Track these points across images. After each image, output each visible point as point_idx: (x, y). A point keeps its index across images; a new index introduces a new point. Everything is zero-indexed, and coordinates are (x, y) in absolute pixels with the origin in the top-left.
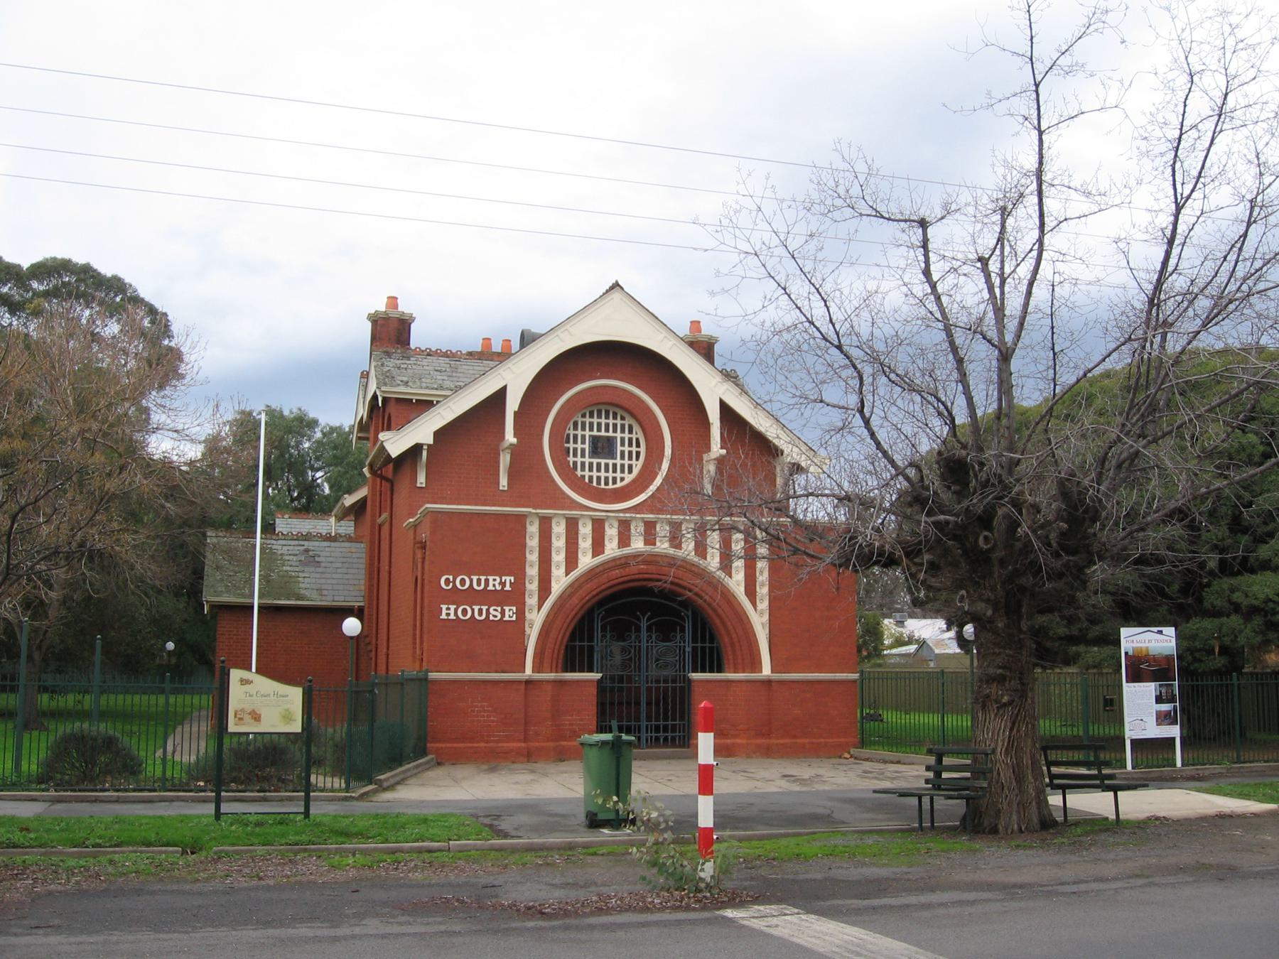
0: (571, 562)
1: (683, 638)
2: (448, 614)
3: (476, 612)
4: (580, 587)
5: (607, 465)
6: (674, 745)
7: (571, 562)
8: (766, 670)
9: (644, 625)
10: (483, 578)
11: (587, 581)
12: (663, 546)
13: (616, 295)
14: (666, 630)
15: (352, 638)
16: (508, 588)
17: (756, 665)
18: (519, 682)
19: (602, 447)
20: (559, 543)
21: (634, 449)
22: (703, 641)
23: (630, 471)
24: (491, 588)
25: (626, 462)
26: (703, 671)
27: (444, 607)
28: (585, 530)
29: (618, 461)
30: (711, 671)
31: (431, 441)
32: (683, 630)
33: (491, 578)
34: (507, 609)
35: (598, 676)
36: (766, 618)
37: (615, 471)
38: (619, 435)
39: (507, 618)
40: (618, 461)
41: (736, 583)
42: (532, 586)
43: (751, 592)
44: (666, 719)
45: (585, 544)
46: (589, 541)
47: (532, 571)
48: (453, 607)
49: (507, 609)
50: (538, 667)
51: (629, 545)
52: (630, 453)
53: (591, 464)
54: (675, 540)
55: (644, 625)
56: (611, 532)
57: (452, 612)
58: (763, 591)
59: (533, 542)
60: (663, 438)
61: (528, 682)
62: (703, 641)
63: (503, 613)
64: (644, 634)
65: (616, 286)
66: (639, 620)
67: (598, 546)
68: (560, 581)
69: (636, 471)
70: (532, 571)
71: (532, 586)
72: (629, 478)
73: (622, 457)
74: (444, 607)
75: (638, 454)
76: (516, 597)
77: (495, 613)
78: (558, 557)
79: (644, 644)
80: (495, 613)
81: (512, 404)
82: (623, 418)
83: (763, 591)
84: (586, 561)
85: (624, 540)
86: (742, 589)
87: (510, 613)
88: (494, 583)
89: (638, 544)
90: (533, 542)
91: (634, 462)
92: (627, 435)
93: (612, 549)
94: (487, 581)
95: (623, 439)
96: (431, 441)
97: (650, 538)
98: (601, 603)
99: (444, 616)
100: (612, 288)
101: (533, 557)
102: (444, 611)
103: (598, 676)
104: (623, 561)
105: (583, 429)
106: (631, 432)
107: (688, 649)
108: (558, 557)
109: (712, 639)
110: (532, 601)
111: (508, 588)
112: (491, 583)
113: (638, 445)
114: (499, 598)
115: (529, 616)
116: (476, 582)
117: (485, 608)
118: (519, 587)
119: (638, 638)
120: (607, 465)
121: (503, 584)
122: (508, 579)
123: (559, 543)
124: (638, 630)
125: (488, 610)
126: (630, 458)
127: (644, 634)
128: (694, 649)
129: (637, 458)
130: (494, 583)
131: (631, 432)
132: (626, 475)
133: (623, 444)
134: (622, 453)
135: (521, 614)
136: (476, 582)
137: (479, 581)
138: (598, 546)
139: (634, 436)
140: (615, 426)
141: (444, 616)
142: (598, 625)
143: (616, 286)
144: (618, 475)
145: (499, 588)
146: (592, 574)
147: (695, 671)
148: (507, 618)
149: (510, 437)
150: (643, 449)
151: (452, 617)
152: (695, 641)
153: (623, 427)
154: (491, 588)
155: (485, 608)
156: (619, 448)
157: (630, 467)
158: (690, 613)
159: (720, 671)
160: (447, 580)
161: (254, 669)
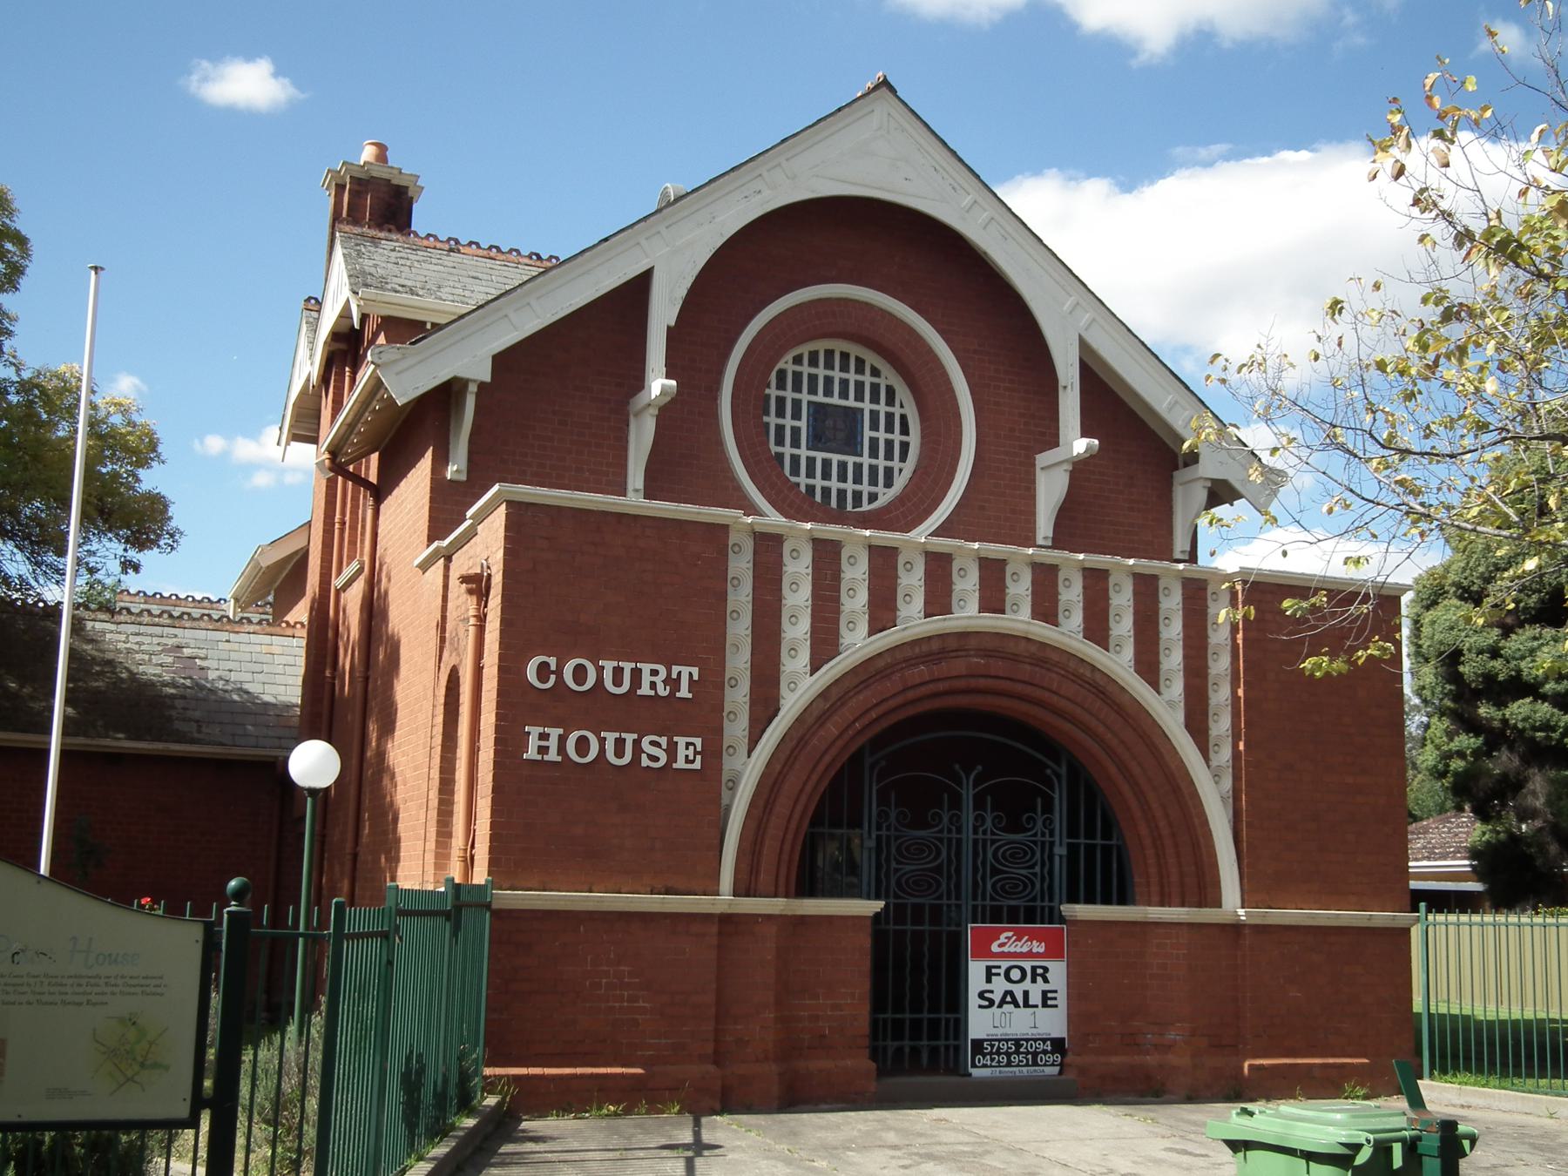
0: (824, 644)
1: (1048, 823)
2: (543, 750)
3: (607, 745)
4: (842, 700)
5: (843, 466)
6: (916, 1069)
7: (824, 644)
8: (1232, 905)
9: (968, 793)
10: (628, 667)
11: (865, 684)
12: (1019, 619)
13: (884, 105)
14: (1015, 808)
15: (313, 792)
16: (684, 692)
17: (1208, 894)
18: (707, 917)
19: (835, 429)
20: (798, 597)
21: (897, 437)
22: (1090, 834)
23: (889, 483)
24: (645, 690)
25: (881, 463)
26: (1090, 900)
27: (534, 731)
28: (856, 574)
29: (866, 460)
30: (1107, 901)
31: (486, 376)
32: (1048, 808)
33: (646, 668)
34: (681, 741)
35: (878, 905)
36: (1227, 783)
37: (858, 479)
38: (867, 406)
39: (680, 764)
40: (866, 460)
41: (1166, 707)
42: (738, 697)
43: (1197, 723)
44: (916, 1008)
45: (855, 601)
46: (863, 596)
47: (739, 662)
48: (555, 733)
49: (681, 741)
50: (743, 888)
51: (947, 610)
52: (889, 444)
53: (811, 462)
54: (1046, 609)
55: (968, 793)
56: (912, 582)
57: (553, 743)
58: (1221, 725)
59: (741, 598)
60: (958, 416)
61: (727, 921)
62: (1090, 834)
63: (672, 751)
64: (968, 816)
65: (885, 83)
66: (960, 784)
67: (882, 611)
68: (801, 686)
69: (900, 482)
70: (739, 662)
71: (738, 697)
72: (886, 496)
73: (874, 453)
74: (534, 731)
75: (905, 447)
76: (700, 717)
77: (653, 751)
78: (797, 630)
79: (968, 836)
80: (653, 751)
81: (663, 311)
82: (875, 372)
83: (1221, 725)
84: (858, 642)
85: (938, 601)
86: (1180, 716)
87: (688, 753)
88: (653, 679)
89: (967, 613)
90: (741, 598)
91: (896, 464)
92: (882, 408)
93: (913, 620)
94: (636, 674)
95: (874, 415)
96: (486, 376)
97: (993, 599)
98: (877, 742)
99: (531, 753)
100: (876, 88)
101: (740, 630)
102: (533, 743)
103: (878, 905)
104: (935, 646)
105: (797, 387)
106: (890, 401)
107: (1060, 850)
108: (797, 630)
109: (1109, 828)
110: (736, 728)
111: (684, 692)
112: (646, 678)
113: (905, 430)
114: (663, 715)
115: (730, 764)
116: (607, 673)
117: (630, 738)
118: (711, 686)
119: (956, 821)
120: (843, 466)
121: (674, 683)
122: (687, 673)
123: (798, 597)
124: (956, 802)
125: (637, 743)
126: (889, 456)
127: (968, 816)
128: (1073, 850)
129: (903, 458)
130: (653, 679)
131: (890, 401)
132: (880, 489)
133: (874, 426)
134: (874, 442)
135: (713, 753)
136: (607, 673)
137: (618, 672)
138: (882, 611)
139: (897, 411)
140: (860, 386)
141: (531, 753)
142: (871, 792)
143: (885, 83)
144: (865, 488)
145: (663, 691)
146: (869, 672)
147: (1073, 899)
148: (680, 764)
149: (658, 384)
150: (914, 439)
151: (553, 756)
152: (1073, 832)
153: (875, 389)
154: (645, 690)
155: (630, 738)
156: (868, 434)
157: (889, 472)
158: (1063, 771)
159: (1123, 901)
160: (543, 667)
161: (44, 868)
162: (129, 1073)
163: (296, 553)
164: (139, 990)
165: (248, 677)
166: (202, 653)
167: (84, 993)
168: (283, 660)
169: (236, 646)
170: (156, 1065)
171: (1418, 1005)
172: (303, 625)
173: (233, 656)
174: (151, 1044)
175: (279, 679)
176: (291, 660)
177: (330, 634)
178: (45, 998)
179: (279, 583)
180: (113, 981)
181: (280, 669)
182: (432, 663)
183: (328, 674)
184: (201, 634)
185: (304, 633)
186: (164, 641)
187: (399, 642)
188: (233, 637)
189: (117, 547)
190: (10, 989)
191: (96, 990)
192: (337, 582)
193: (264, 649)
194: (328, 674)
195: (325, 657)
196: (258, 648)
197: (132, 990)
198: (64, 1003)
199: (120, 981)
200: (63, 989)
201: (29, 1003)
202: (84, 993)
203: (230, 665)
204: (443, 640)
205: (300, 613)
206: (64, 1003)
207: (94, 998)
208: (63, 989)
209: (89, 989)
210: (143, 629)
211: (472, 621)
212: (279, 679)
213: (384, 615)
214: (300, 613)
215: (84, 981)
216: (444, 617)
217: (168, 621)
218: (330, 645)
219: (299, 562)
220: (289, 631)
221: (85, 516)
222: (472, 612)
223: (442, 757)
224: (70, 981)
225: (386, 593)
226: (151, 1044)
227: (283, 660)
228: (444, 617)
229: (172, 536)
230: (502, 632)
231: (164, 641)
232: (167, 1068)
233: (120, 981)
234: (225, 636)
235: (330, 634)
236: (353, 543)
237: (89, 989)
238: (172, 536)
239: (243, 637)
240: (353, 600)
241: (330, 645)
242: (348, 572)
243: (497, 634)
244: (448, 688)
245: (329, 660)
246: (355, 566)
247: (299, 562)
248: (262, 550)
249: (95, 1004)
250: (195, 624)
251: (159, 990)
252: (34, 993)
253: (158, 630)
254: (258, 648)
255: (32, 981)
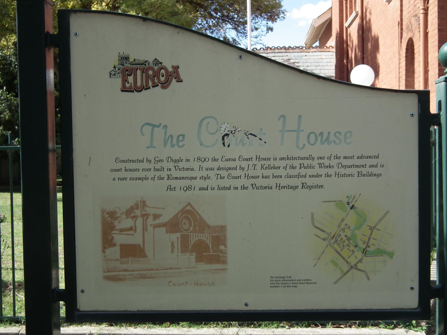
162: (353, 261)
163: (326, 21)
164: (354, 171)
165: (314, 68)
166: (297, 61)
167: (299, 176)
168: (326, 60)
169: (309, 57)
170: (380, 252)
171: (18, 198)
172: (332, 47)
173: (308, 61)
174: (372, 229)
175: (325, 68)
176: (329, 60)
177: (345, 45)
178: (260, 182)
179: (322, 32)
180: (326, 162)
181: (326, 64)
182: (397, 41)
183: (345, 62)
184: (296, 54)
185: (334, 50)
186: (283, 58)
187: (378, 38)
188: (307, 54)
189: (264, 22)
190: (224, 173)
191: (310, 172)
192: (346, 25)
193: (319, 57)
194: (345, 62)
195: (343, 55)
196: (317, 57)
197: (348, 171)
198: (279, 187)
199: (334, 162)
200: (277, 172)
201: (244, 188)
202: (299, 176)
203: (307, 64)
204: (402, 29)
205: (332, 42)
206: (279, 187)
207: (310, 181)
208: (277, 172)
209: (303, 172)
210: (276, 54)
211: (422, 11)
212: (325, 68)
213: (369, 29)
214: (332, 42)
215: (296, 163)
216: (402, 19)
217: (284, 51)
218: (345, 50)
219: (329, 24)
220: (328, 50)
221: (253, 12)
222: (421, 7)
223: (406, 81)
224: (283, 163)
225: (370, 20)
226: (372, 229)
227: (326, 60)
228: (402, 19)
229: (284, 13)
230: (439, 12)
231: (283, 58)
232: (391, 255)
233: (334, 162)
234: (304, 54)
235: (345, 45)
236: (351, 8)
237: (303, 172)
238: (284, 13)
239: (311, 54)
240: (353, 32)
241: (345, 50)
242: (350, 19)
243: (436, 14)
244: (407, 49)
245: (345, 56)
246: (354, 14)
247: (329, 24)
248: (315, 20)
249: (311, 187)
250: (294, 51)
251: (375, 171)
252: (248, 177)
253: (281, 54)
254: (317, 57)
255: (244, 164)
